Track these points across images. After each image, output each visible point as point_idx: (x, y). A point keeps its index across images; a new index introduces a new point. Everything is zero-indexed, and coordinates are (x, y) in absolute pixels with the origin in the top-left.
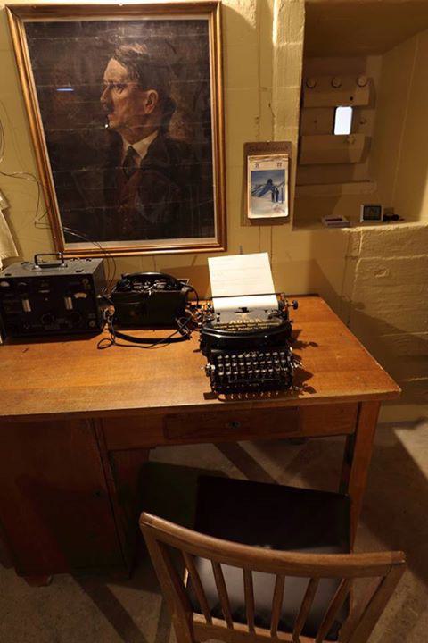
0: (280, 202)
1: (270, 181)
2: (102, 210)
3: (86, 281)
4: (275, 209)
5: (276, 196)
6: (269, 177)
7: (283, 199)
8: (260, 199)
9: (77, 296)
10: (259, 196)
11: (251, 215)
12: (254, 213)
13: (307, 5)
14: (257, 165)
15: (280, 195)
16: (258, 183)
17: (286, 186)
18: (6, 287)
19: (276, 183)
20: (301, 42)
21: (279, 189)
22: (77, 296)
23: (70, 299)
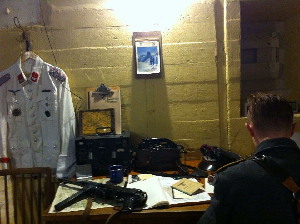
0: (155, 65)
1: (149, 53)
2: (231, 121)
3: (125, 142)
4: (153, 69)
5: (153, 62)
6: (148, 50)
7: (157, 63)
8: (144, 63)
9: (119, 150)
10: (143, 61)
11: (139, 73)
12: (140, 71)
13: (241, 3)
14: (141, 44)
15: (155, 61)
16: (142, 54)
17: (159, 56)
18: (212, 168)
19: (153, 54)
20: (239, 19)
21: (155, 58)
22: (119, 150)
23: (115, 152)
